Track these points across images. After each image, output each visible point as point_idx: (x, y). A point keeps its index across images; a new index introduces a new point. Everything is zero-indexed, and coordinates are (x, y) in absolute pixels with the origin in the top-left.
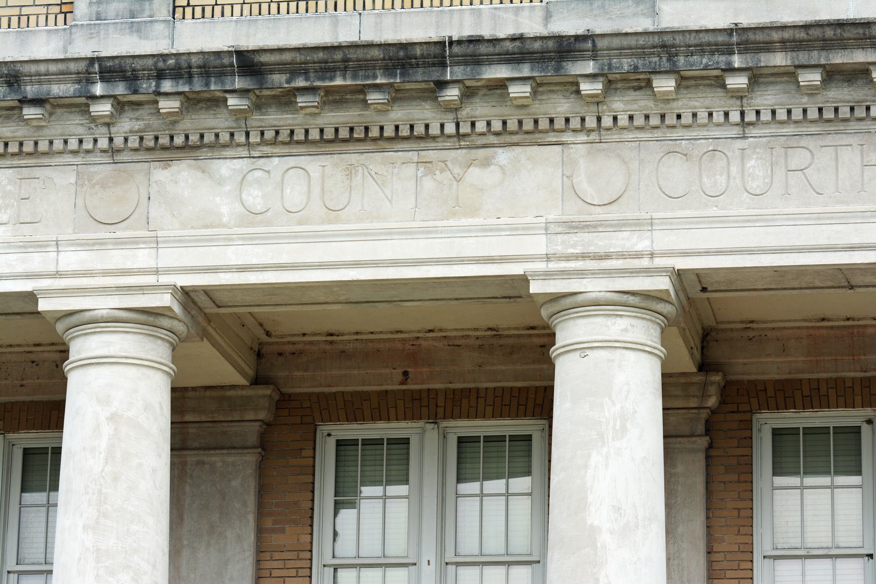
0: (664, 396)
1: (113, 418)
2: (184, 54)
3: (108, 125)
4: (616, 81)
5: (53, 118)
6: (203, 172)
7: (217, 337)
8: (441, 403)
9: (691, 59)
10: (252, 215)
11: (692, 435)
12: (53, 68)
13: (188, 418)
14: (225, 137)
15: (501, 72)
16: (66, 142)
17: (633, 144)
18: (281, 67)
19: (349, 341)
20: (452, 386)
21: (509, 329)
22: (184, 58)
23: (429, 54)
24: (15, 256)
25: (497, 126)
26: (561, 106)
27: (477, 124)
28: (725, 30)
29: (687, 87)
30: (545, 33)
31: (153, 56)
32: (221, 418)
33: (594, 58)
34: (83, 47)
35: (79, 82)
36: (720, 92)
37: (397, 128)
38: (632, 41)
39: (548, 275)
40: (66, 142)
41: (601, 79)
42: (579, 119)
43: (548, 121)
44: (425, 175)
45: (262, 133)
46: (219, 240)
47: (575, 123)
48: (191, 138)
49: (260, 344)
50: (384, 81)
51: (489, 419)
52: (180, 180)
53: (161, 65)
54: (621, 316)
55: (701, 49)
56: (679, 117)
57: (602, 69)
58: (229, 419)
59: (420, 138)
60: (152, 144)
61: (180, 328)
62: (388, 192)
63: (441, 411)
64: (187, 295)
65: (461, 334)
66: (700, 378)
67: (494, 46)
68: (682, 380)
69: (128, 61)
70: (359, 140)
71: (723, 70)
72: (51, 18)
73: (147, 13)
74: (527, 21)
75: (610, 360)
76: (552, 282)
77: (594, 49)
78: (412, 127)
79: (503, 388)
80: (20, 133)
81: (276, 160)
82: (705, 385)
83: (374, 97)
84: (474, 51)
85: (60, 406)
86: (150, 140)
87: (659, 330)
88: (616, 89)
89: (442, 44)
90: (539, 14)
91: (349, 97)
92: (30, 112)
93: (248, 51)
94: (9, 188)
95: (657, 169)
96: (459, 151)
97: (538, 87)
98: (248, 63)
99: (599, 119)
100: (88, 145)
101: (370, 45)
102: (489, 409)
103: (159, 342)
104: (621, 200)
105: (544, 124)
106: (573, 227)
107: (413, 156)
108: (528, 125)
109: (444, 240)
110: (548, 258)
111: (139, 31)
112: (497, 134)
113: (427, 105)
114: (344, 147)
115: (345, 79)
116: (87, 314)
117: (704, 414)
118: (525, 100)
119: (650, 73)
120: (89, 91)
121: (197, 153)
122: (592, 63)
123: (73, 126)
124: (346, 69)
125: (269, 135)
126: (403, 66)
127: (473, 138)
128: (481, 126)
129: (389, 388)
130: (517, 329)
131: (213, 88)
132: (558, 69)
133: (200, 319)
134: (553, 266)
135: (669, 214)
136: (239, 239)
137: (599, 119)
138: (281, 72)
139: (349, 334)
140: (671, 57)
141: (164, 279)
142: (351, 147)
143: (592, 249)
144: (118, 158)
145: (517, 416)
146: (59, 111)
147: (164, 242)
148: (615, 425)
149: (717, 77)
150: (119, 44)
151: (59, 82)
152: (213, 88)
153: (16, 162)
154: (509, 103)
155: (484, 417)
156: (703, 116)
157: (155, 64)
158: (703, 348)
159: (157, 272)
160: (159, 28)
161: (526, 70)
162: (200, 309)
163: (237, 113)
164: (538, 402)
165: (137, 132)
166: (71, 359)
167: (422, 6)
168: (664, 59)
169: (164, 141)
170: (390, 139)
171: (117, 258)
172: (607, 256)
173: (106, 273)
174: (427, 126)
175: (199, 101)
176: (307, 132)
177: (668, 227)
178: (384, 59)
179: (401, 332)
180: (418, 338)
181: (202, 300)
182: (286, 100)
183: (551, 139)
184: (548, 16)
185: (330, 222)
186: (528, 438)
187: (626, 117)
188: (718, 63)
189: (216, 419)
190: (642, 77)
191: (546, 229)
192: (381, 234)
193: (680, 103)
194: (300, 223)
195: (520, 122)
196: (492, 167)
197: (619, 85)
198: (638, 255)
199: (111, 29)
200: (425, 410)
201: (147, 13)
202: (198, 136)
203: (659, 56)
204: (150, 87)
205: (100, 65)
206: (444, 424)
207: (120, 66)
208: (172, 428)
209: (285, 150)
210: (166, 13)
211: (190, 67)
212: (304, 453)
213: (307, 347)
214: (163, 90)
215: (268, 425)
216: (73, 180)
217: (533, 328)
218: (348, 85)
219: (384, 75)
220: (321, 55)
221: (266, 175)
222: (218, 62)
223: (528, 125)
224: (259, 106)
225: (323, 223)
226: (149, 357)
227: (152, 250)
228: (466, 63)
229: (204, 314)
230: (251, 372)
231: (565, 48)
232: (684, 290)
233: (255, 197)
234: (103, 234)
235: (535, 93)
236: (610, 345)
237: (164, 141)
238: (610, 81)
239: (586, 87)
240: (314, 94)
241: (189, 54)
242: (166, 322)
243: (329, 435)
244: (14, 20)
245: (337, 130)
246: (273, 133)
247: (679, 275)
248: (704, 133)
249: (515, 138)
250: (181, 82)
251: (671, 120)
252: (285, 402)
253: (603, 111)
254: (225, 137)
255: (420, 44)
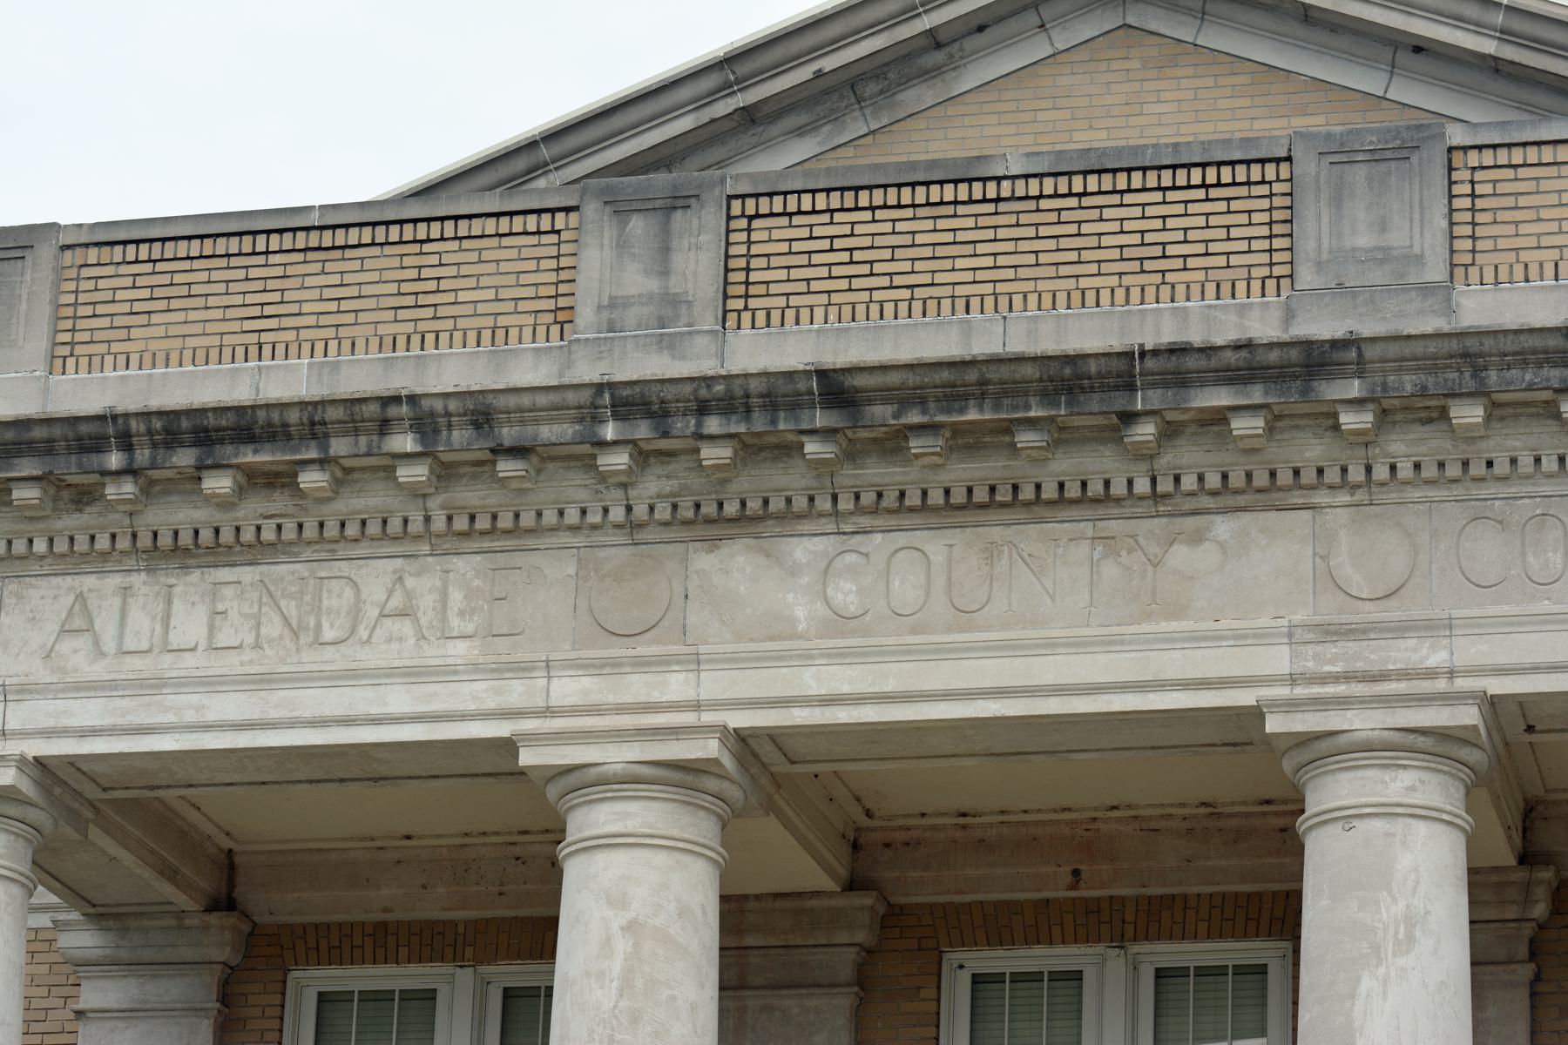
0: (1473, 903)
1: (632, 927)
2: (738, 376)
3: (624, 486)
4: (1394, 411)
5: (542, 477)
6: (768, 556)
7: (791, 814)
8: (1130, 918)
9: (1508, 374)
10: (840, 622)
11: (1510, 962)
12: (542, 400)
13: (750, 941)
14: (800, 503)
15: (1220, 397)
16: (561, 513)
17: (1420, 507)
18: (886, 395)
19: (991, 825)
20: (1143, 891)
21: (1233, 804)
22: (739, 381)
23: (1109, 372)
24: (484, 685)
25: (1213, 481)
26: (1311, 450)
27: (1184, 479)
28: (1558, 329)
29: (1502, 418)
30: (1286, 338)
31: (692, 379)
32: (799, 942)
33: (1360, 374)
34: (587, 371)
35: (581, 420)
36: (1552, 425)
37: (1061, 485)
38: (1418, 348)
39: (1292, 705)
40: (561, 513)
41: (1371, 406)
42: (1337, 470)
43: (1291, 473)
44: (1105, 557)
45: (857, 497)
46: (791, 657)
47: (1333, 475)
48: (749, 504)
49: (857, 830)
50: (1040, 414)
51: (1202, 940)
52: (734, 572)
53: (703, 393)
54: (1405, 767)
55: (1523, 358)
56: (1490, 464)
57: (1373, 391)
58: (812, 942)
59: (1096, 501)
60: (690, 514)
61: (734, 793)
62: (1048, 584)
63: (1130, 929)
64: (743, 742)
65: (1159, 812)
66: (1521, 874)
67: (1209, 358)
68: (1494, 878)
69: (655, 388)
70: (1003, 505)
71: (1556, 391)
72: (541, 330)
73: (684, 320)
74: (1257, 325)
75: (1388, 835)
76: (1299, 715)
77: (1361, 360)
78: (1084, 484)
79: (1224, 895)
80: (492, 500)
81: (878, 537)
82: (1528, 886)
83: (1025, 438)
84: (1178, 365)
85: (550, 925)
86: (687, 509)
87: (1462, 790)
88: (1394, 423)
89: (1127, 355)
90: (1276, 315)
91: (988, 439)
92: (507, 467)
93: (835, 371)
94: (476, 582)
95: (1458, 544)
96: (1156, 520)
97: (1276, 420)
98: (836, 389)
99: (1369, 469)
100: (595, 518)
101: (1020, 359)
102: (1203, 927)
103: (702, 813)
104: (1403, 591)
105: (1285, 477)
106: (1330, 632)
107: (1087, 528)
108: (1261, 479)
109: (1133, 655)
110: (1293, 680)
111: (671, 347)
112: (1214, 493)
113: (1107, 450)
114: (981, 516)
115: (981, 410)
116: (593, 770)
117: (1528, 930)
118: (1255, 440)
119: (1446, 396)
120: (595, 434)
121: (760, 528)
122: (1356, 382)
123: (573, 488)
124: (983, 396)
125: (868, 498)
126: (1070, 391)
127: (1178, 499)
128: (1189, 482)
129: (1051, 895)
130: (1244, 803)
131: (782, 427)
132: (1305, 392)
133: (765, 781)
134: (1300, 691)
135: (1476, 612)
136: (822, 655)
137: (1369, 469)
138: (886, 401)
139: (991, 813)
140: (1477, 371)
141: (708, 718)
142: (992, 515)
143: (1360, 665)
144: (640, 536)
145: (1245, 936)
146: (551, 466)
147: (708, 661)
148: (1397, 933)
149: (1546, 402)
150: (642, 364)
151: (552, 421)
152: (782, 427)
153: (486, 544)
154: (1231, 446)
155: (1195, 937)
156: (1526, 462)
157: (696, 390)
158: (1525, 830)
159: (697, 706)
160: (702, 342)
161: (1256, 395)
162: (764, 765)
163: (817, 464)
164: (1280, 915)
165: (667, 496)
166: (569, 839)
167: (1098, 305)
168: (1467, 375)
169: (709, 509)
170: (1050, 503)
171: (638, 687)
172: (1383, 676)
173: (621, 709)
174: (1107, 483)
175: (761, 449)
176: (925, 493)
177: (1477, 631)
178: (1041, 380)
179: (1069, 810)
180: (1095, 819)
181: (768, 752)
182: (893, 444)
183: (1295, 501)
184: (1289, 315)
185: (961, 630)
186: (1262, 970)
187: (1410, 465)
188: (1548, 379)
189: (791, 943)
190: (1433, 403)
191: (1290, 635)
192: (1037, 646)
193: (1492, 443)
194: (914, 631)
195: (1249, 475)
196: (1207, 544)
197: (1399, 417)
198: (1431, 674)
199: (630, 345)
200: (1105, 928)
201: (684, 320)
202: (760, 502)
203: (1458, 370)
204: (687, 426)
205: (612, 395)
206: (1135, 948)
207: (643, 396)
208: (720, 956)
209: (893, 521)
210: (712, 319)
211: (748, 396)
212: (924, 993)
213: (928, 834)
214: (706, 431)
215: (869, 951)
216: (571, 570)
217: (1268, 802)
218: (986, 421)
219: (1042, 405)
220: (945, 375)
221: (862, 560)
222: (789, 388)
223: (1261, 479)
224: (852, 454)
225: (949, 631)
226: (686, 836)
227: (691, 675)
228: (1166, 385)
229: (768, 778)
230: (844, 873)
231: (1315, 361)
232: (1500, 729)
233: (845, 594)
234: (618, 651)
235: (1270, 429)
236: (1388, 812)
237: (709, 509)
238: (1384, 411)
239: (1348, 419)
240: (936, 435)
241: (746, 375)
242: (711, 784)
243: (961, 967)
244: (486, 335)
245: (970, 490)
246: (873, 496)
247: (1493, 705)
248: (1529, 489)
249: (1241, 500)
250: (734, 418)
251: (1477, 469)
252: (893, 918)
253: (1375, 457)
254: (800, 503)
255: (1096, 355)
